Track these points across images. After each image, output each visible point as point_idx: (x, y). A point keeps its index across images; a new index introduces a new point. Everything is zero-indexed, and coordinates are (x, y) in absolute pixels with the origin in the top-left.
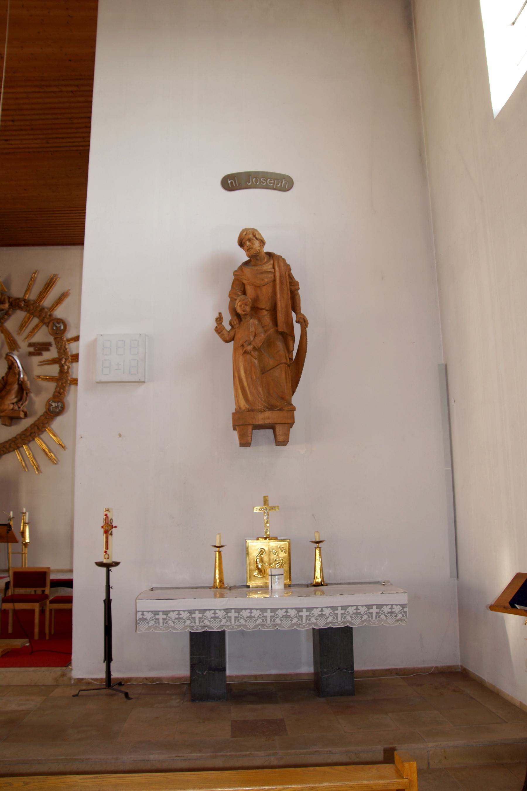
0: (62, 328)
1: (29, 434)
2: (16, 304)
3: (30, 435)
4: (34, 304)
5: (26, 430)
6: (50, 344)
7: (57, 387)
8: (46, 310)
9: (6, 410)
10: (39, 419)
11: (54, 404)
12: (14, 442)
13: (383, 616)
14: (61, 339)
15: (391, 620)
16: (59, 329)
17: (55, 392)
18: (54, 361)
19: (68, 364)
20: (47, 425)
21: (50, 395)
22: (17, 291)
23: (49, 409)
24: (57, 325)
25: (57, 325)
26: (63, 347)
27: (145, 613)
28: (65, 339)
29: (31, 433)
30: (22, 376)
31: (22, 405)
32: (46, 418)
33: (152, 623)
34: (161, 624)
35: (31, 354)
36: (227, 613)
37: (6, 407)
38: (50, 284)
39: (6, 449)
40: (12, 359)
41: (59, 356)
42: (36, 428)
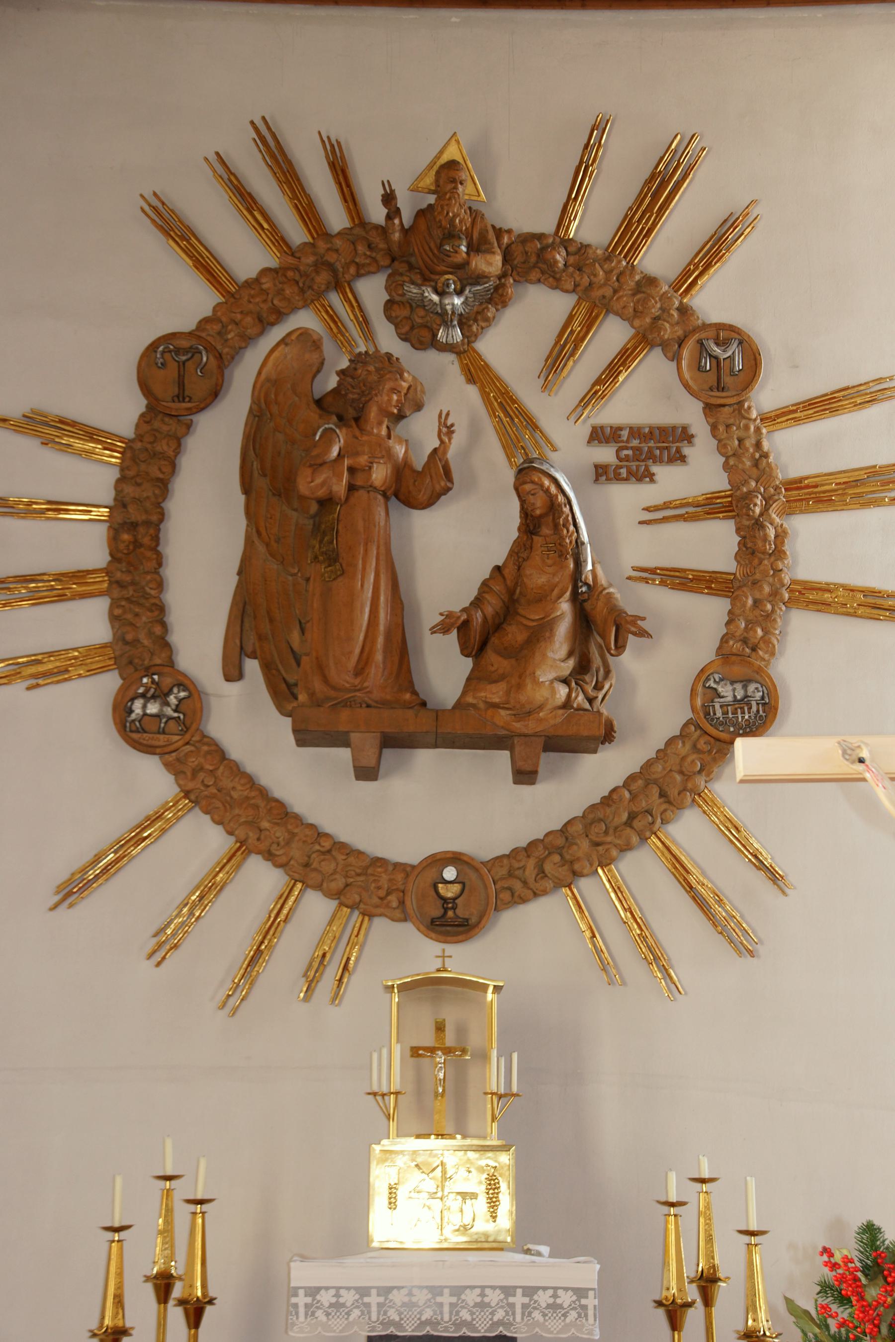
0: (738, 365)
1: (625, 816)
2: (533, 258)
3: (629, 823)
4: (608, 258)
5: (607, 801)
6: (686, 435)
9: (541, 707)
10: (661, 754)
11: (726, 691)
12: (559, 850)
13: (537, 1315)
14: (740, 409)
15: (555, 1325)
16: (723, 368)
17: (724, 640)
18: (709, 508)
19: (777, 520)
21: (704, 651)
22: (519, 203)
24: (717, 350)
25: (717, 350)
26: (749, 443)
28: (754, 414)
29: (632, 817)
31: (598, 687)
33: (573, 1315)
34: (518, 1318)
35: (601, 473)
37: (540, 695)
38: (659, 189)
39: (525, 883)
40: (553, 490)
41: (735, 486)
42: (655, 791)
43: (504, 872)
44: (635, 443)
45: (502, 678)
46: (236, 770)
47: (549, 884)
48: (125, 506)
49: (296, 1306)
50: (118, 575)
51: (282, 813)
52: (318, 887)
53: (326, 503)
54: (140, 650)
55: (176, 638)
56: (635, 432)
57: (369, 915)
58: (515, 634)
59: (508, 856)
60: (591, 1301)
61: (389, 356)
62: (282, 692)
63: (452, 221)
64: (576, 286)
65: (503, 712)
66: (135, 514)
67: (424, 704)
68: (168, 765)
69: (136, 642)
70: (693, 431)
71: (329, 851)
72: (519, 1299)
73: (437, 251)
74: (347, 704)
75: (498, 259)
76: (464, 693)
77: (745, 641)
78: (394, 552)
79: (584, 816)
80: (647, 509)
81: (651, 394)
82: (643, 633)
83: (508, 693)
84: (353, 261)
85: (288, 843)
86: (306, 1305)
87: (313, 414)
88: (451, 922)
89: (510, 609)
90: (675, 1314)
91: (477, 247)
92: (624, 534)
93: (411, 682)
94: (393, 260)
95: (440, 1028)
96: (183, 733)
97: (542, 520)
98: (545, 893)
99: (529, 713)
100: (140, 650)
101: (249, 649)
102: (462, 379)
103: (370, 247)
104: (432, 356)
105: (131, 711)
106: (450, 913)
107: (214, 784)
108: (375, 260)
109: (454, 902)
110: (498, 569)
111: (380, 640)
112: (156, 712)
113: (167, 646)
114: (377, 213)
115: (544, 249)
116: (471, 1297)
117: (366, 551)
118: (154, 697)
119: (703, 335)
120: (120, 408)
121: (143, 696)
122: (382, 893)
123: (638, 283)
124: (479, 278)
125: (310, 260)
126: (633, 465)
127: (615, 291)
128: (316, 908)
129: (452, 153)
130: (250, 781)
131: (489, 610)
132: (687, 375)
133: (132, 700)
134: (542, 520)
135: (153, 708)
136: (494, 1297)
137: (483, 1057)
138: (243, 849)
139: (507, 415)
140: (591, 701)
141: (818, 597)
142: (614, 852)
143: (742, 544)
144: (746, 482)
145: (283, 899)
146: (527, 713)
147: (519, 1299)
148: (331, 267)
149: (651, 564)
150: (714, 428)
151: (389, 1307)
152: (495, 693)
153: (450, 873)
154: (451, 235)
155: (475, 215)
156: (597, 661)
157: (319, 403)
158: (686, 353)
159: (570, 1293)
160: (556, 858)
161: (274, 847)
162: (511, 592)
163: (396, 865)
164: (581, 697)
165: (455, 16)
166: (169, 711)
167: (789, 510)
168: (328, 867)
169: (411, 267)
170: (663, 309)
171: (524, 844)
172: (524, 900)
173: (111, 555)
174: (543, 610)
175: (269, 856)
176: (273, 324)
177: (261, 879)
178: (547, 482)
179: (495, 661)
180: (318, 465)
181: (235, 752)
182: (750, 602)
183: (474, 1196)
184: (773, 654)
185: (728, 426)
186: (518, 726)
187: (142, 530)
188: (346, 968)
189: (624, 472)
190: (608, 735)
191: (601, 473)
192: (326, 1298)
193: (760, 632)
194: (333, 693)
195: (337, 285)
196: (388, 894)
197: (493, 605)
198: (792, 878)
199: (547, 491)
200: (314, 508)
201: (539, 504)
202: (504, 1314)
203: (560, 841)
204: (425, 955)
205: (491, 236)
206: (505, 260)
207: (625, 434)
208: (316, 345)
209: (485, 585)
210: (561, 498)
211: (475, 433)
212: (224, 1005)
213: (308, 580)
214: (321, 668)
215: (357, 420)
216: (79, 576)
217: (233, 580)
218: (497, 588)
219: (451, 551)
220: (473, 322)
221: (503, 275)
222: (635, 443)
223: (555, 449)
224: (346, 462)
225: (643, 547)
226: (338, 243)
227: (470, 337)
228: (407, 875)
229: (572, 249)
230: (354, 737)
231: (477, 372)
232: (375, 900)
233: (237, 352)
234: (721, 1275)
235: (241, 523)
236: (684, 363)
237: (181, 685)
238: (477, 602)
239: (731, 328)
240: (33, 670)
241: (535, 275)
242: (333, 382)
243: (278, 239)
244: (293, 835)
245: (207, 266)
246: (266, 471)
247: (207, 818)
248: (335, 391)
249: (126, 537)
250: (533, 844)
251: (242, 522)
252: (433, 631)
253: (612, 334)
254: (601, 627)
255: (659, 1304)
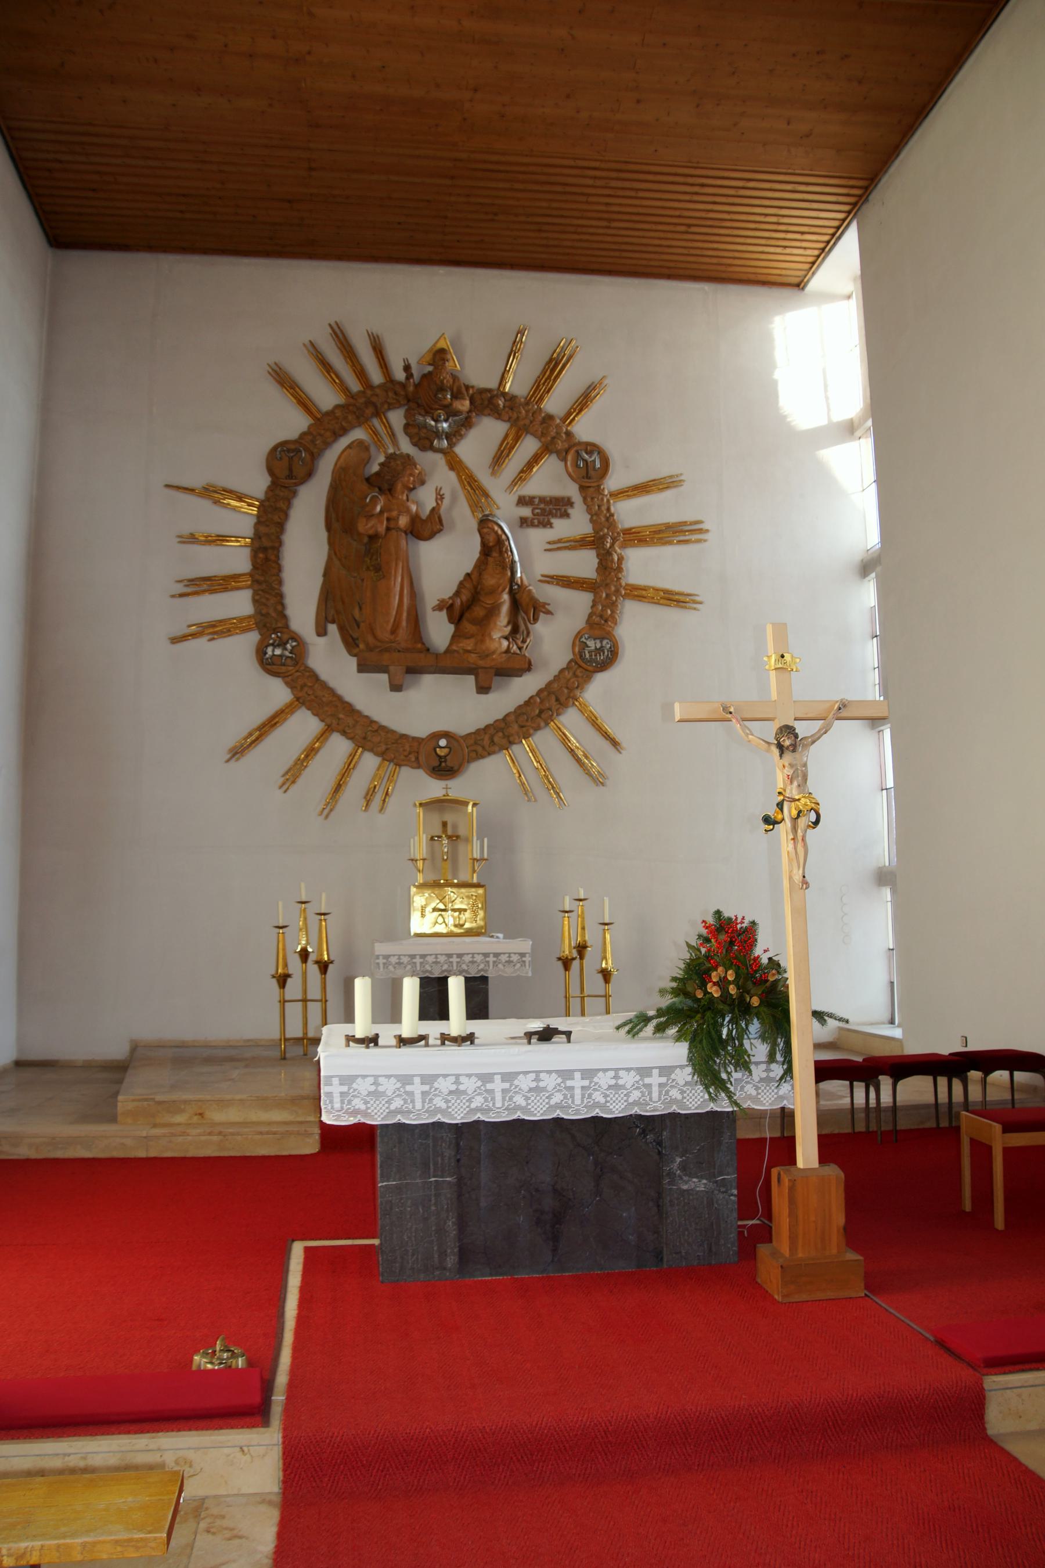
0: (598, 465)
1: (537, 712)
2: (487, 402)
3: (539, 715)
5: (528, 703)
6: (569, 502)
7: (594, 604)
8: (558, 421)
9: (494, 653)
10: (557, 678)
11: (591, 644)
12: (502, 730)
14: (599, 490)
16: (589, 467)
17: (590, 616)
18: (581, 543)
19: (619, 551)
20: (577, 693)
22: (477, 370)
23: (581, 655)
24: (586, 456)
25: (586, 456)
26: (604, 508)
27: (381, 1080)
28: (606, 492)
29: (541, 712)
30: (519, 575)
31: (524, 641)
32: (575, 675)
33: (519, 965)
35: (524, 522)
36: (642, 1077)
37: (493, 646)
38: (553, 368)
39: (483, 747)
40: (500, 532)
41: (596, 531)
42: (553, 698)
43: (472, 742)
44: (542, 506)
45: (472, 636)
46: (324, 686)
47: (497, 748)
48: (260, 538)
49: (378, 964)
50: (257, 577)
51: (349, 709)
52: (371, 750)
53: (373, 538)
54: (270, 619)
55: (290, 612)
56: (542, 500)
57: (399, 765)
58: (479, 612)
59: (474, 733)
60: (527, 959)
61: (408, 456)
62: (351, 643)
63: (442, 382)
64: (510, 418)
65: (473, 655)
66: (266, 543)
67: (428, 650)
68: (287, 683)
69: (267, 615)
70: (573, 500)
71: (376, 731)
72: (491, 959)
73: (433, 397)
74: (387, 650)
75: (467, 403)
76: (451, 644)
77: (601, 616)
78: (411, 564)
79: (515, 711)
80: (549, 543)
81: (550, 479)
82: (549, 612)
83: (476, 644)
84: (386, 401)
85: (354, 726)
86: (504, 1091)
87: (365, 486)
88: (443, 769)
89: (475, 598)
90: (566, 963)
91: (456, 396)
92: (537, 557)
93: (421, 638)
94: (409, 401)
95: (444, 824)
96: (295, 665)
97: (493, 549)
98: (494, 753)
99: (487, 656)
100: (270, 619)
101: (330, 618)
102: (446, 468)
103: (396, 393)
104: (430, 456)
105: (266, 653)
106: (443, 764)
107: (312, 693)
108: (398, 401)
109: (445, 757)
110: (468, 575)
111: (405, 614)
112: (280, 653)
113: (285, 617)
114: (400, 375)
115: (492, 397)
116: (525, 1083)
117: (396, 565)
118: (279, 645)
119: (578, 448)
120: (258, 483)
121: (272, 645)
122: (406, 753)
123: (544, 418)
124: (456, 413)
125: (362, 400)
126: (541, 518)
127: (531, 422)
128: (369, 762)
129: (442, 344)
130: (332, 692)
131: (464, 598)
132: (570, 469)
133: (266, 647)
134: (493, 549)
135: (278, 652)
136: (628, 1079)
137: (468, 840)
138: (328, 730)
139: (472, 488)
140: (520, 649)
141: (638, 593)
142: (531, 731)
143: (600, 563)
144: (602, 530)
145: (352, 755)
146: (486, 655)
147: (491, 959)
148: (374, 405)
149: (552, 573)
150: (585, 499)
151: (435, 1095)
152: (468, 644)
153: (443, 742)
154: (442, 389)
155: (455, 378)
156: (522, 627)
157: (368, 480)
158: (569, 458)
159: (393, 1080)
160: (500, 734)
161: (347, 729)
162: (475, 588)
163: (414, 738)
164: (515, 647)
165: (441, 272)
166: (287, 653)
167: (623, 546)
168: (376, 739)
169: (419, 406)
170: (557, 433)
171: (482, 726)
172: (483, 757)
173: (253, 565)
174: (491, 596)
175: (344, 733)
176: (341, 436)
177: (339, 746)
178: (496, 528)
179: (468, 627)
180: (370, 516)
181: (324, 676)
182: (604, 595)
183: (465, 910)
184: (616, 624)
185: (592, 499)
186: (481, 663)
187: (270, 551)
188: (387, 794)
189: (536, 521)
190: (527, 667)
191: (524, 522)
192: (394, 960)
193: (609, 612)
194: (379, 644)
195: (377, 414)
196: (410, 753)
197: (465, 596)
198: (624, 744)
199: (496, 533)
200: (366, 540)
201: (491, 540)
202: (402, 1102)
203: (503, 725)
204: (435, 788)
205: (463, 390)
206: (471, 403)
207: (537, 501)
208: (367, 449)
209: (461, 583)
210: (504, 537)
211: (454, 499)
212: (322, 812)
213: (363, 580)
214: (372, 631)
215: (390, 490)
216: (235, 577)
217: (319, 580)
218: (468, 585)
219: (442, 565)
220: (454, 436)
221: (470, 411)
222: (542, 506)
223: (498, 508)
224: (386, 515)
225: (548, 563)
226: (378, 391)
227: (451, 445)
228: (420, 744)
229: (507, 398)
230: (392, 668)
231: (455, 464)
232: (402, 757)
233: (321, 452)
234: (589, 944)
235: (325, 548)
236: (569, 463)
237: (294, 639)
238: (457, 593)
239: (593, 445)
240: (211, 630)
241: (487, 411)
242: (375, 468)
243: (344, 388)
244: (357, 722)
245: (305, 403)
246: (340, 518)
247: (309, 713)
248: (377, 474)
249: (261, 555)
250: (488, 727)
251: (326, 547)
252: (434, 609)
253: (529, 445)
254: (526, 608)
255: (559, 959)
